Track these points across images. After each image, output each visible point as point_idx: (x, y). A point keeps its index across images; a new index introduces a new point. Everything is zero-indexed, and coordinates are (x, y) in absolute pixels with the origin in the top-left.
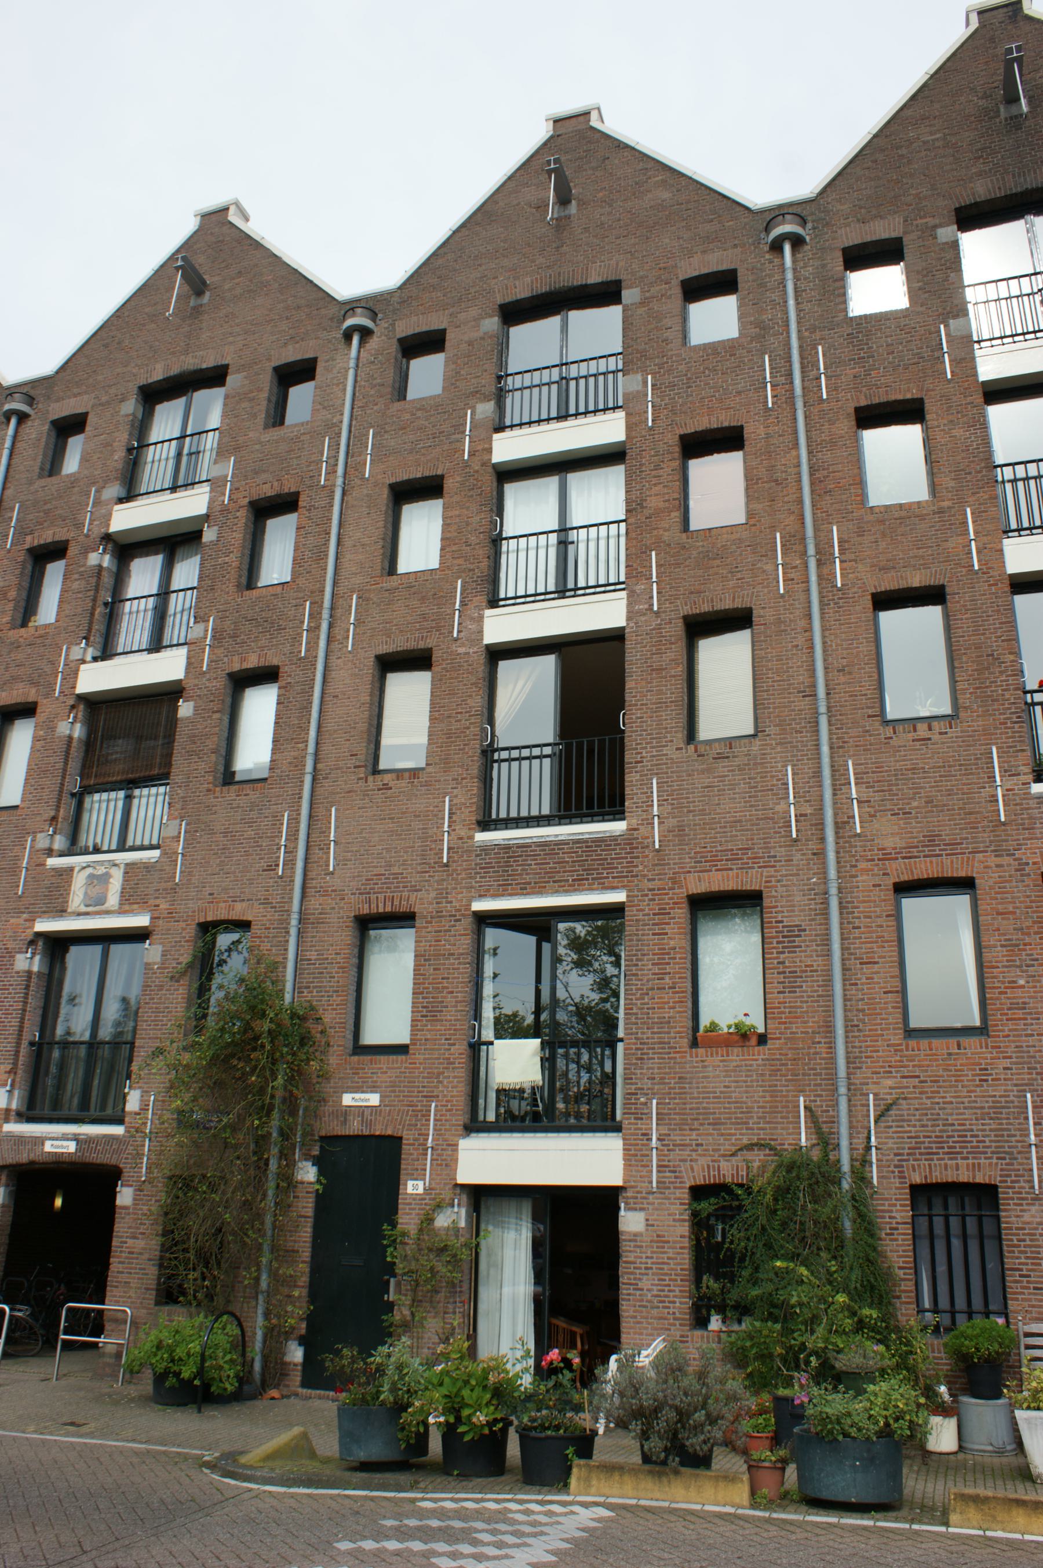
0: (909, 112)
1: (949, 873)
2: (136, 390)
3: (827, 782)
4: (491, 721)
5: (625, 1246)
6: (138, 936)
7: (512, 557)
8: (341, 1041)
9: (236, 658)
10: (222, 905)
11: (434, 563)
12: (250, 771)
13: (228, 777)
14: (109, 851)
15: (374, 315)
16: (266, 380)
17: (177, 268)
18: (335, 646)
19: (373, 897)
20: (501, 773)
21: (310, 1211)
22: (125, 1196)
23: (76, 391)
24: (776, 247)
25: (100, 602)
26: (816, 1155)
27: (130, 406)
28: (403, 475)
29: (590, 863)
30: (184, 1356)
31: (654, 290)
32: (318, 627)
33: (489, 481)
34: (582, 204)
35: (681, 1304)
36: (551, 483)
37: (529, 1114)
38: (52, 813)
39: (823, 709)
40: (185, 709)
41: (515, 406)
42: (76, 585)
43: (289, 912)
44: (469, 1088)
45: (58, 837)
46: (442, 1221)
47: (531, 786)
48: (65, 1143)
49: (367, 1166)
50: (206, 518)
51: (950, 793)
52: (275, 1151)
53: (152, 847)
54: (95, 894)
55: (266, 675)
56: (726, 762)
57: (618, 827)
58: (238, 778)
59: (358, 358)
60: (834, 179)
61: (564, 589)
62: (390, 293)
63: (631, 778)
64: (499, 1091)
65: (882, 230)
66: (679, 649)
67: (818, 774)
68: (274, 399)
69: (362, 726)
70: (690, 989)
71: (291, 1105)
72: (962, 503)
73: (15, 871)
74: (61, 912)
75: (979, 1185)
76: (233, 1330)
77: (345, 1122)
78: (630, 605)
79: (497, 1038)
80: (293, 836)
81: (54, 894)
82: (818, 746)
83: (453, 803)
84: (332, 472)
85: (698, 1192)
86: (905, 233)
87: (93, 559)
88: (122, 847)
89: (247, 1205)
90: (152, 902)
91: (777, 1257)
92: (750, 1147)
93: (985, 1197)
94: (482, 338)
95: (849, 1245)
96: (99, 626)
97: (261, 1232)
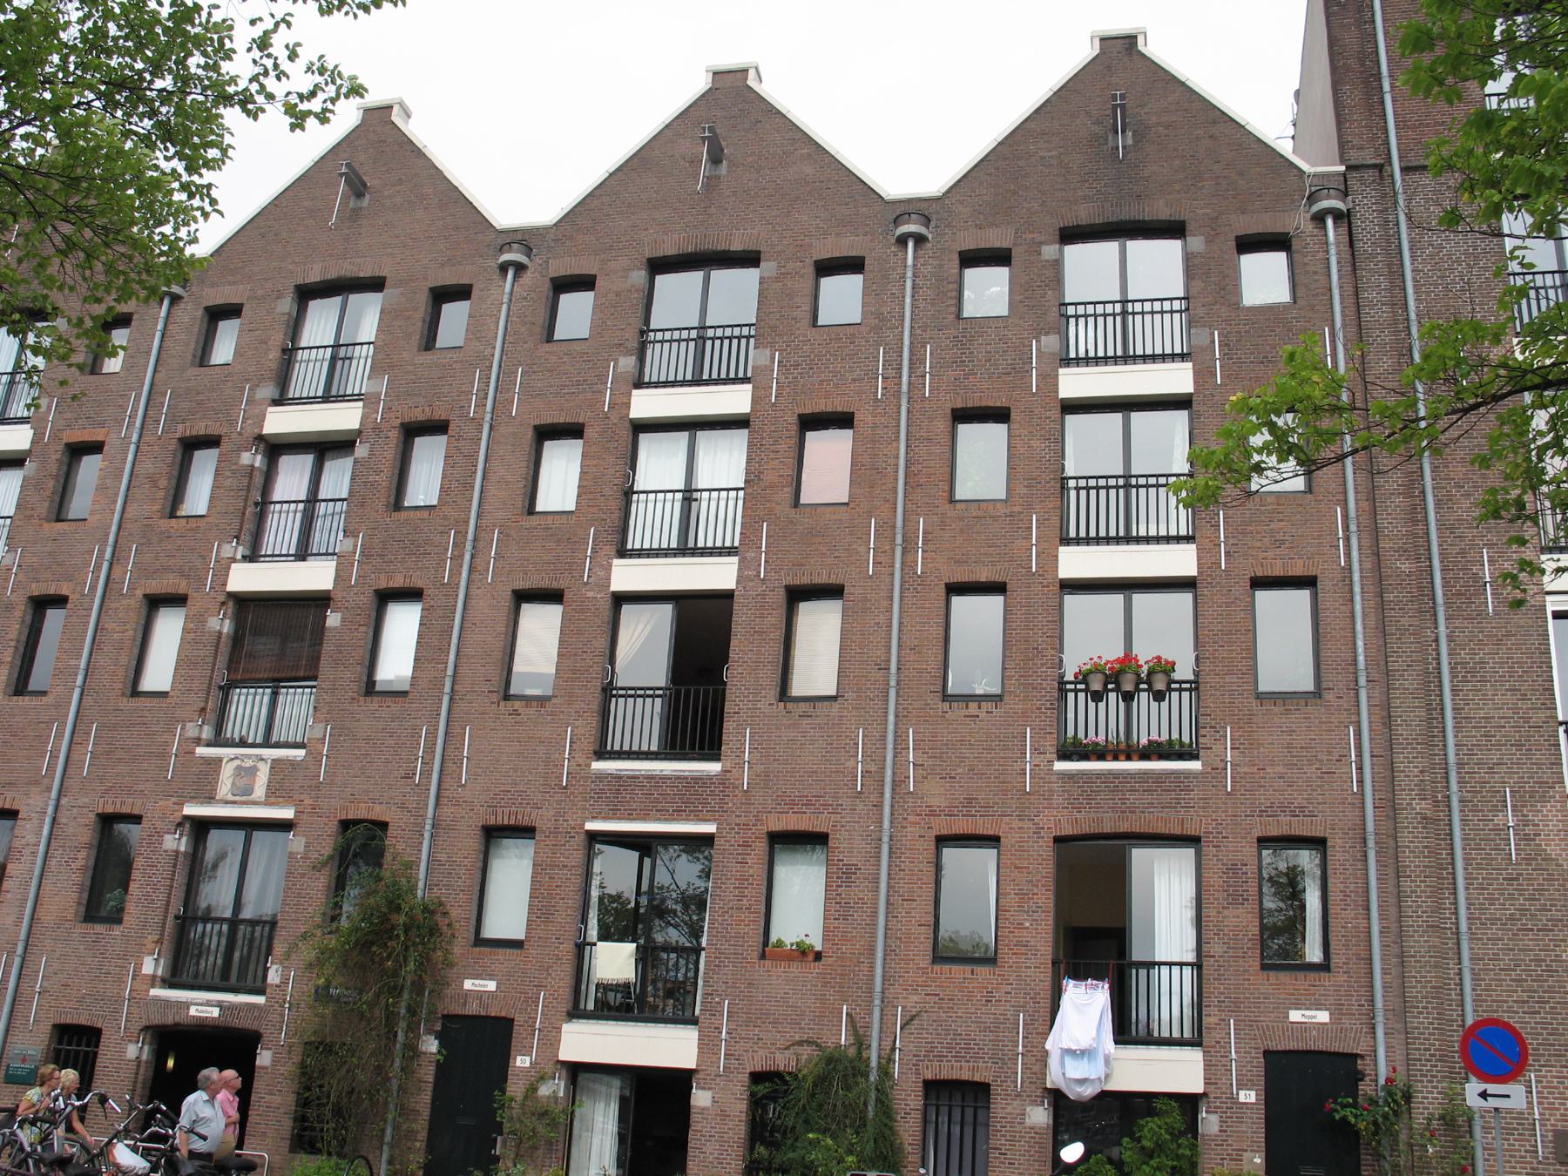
0: (1032, 125)
1: (980, 832)
2: (292, 289)
3: (890, 746)
5: (694, 1117)
6: (284, 826)
7: (642, 506)
8: (465, 934)
9: (382, 576)
11: (570, 505)
12: (391, 682)
13: (370, 688)
14: (253, 746)
16: (423, 300)
17: (341, 175)
19: (500, 811)
20: (618, 707)
24: (902, 241)
25: (250, 503)
26: (852, 1052)
27: (287, 305)
29: (689, 797)
31: (790, 266)
32: (462, 556)
33: (626, 433)
34: (732, 164)
36: (683, 437)
37: (621, 1005)
39: (893, 683)
40: (333, 619)
42: (228, 483)
43: (424, 817)
45: (206, 727)
46: (544, 1090)
47: (641, 722)
49: (482, 1043)
50: (359, 432)
52: (403, 1025)
54: (242, 784)
55: (411, 595)
57: (714, 767)
58: (378, 688)
62: (546, 229)
63: (729, 726)
65: (994, 239)
67: (884, 738)
69: (497, 655)
71: (418, 987)
72: (1030, 507)
73: (164, 756)
74: (210, 799)
77: (465, 1004)
78: (740, 569)
80: (430, 749)
81: (203, 781)
83: (576, 730)
84: (481, 405)
85: (757, 1077)
87: (246, 458)
88: (267, 744)
89: (379, 1069)
90: (297, 797)
91: (812, 1131)
92: (800, 1043)
93: (978, 1092)
95: (869, 1127)
96: (249, 526)
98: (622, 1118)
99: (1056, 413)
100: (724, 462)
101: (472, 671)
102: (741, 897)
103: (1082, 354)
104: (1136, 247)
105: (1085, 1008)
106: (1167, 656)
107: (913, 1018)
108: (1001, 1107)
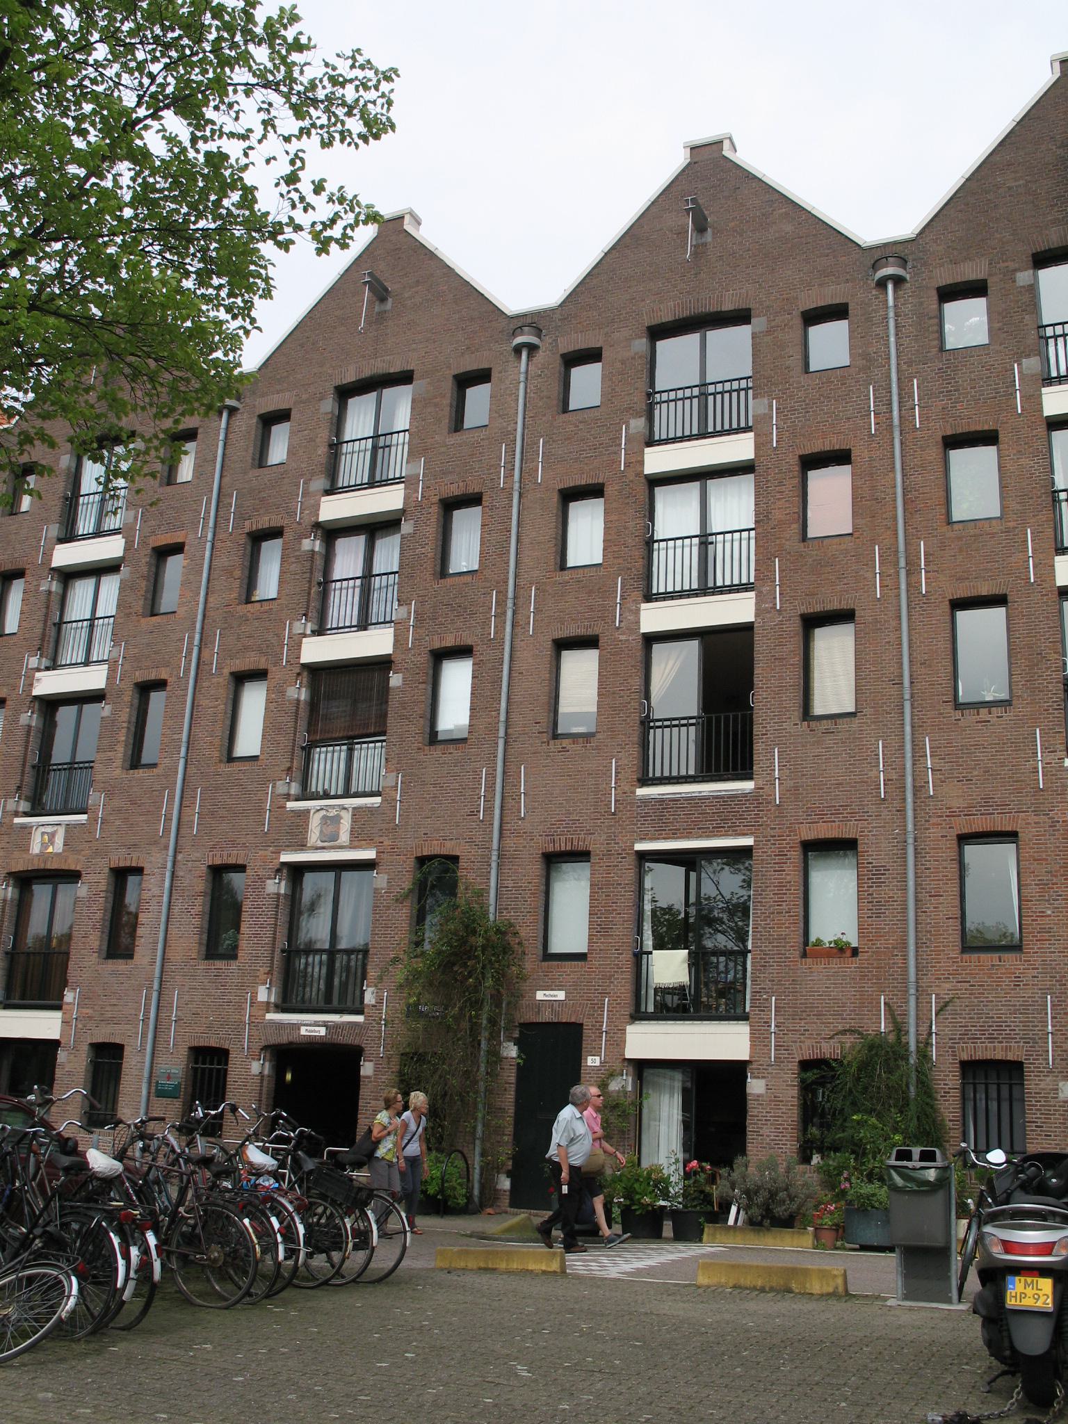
3: (909, 755)
4: (647, 695)
8: (534, 950)
13: (433, 737)
15: (538, 332)
16: (448, 386)
18: (518, 630)
21: (513, 1079)
22: (367, 1069)
23: (278, 387)
24: (882, 284)
26: (892, 1038)
27: (328, 405)
28: (570, 483)
29: (725, 814)
30: (429, 1179)
32: (504, 613)
33: (642, 488)
37: (678, 1006)
38: (288, 765)
39: (907, 696)
40: (395, 680)
43: (489, 849)
44: (634, 987)
45: (293, 784)
47: (679, 748)
48: (317, 1028)
50: (403, 511)
51: (1002, 765)
53: (372, 794)
54: (329, 831)
55: (461, 652)
56: (832, 736)
57: (748, 786)
58: (440, 737)
59: (527, 372)
60: (932, 220)
61: (705, 589)
62: (552, 310)
63: (758, 747)
64: (655, 989)
65: (970, 272)
66: (796, 643)
67: (902, 747)
68: (455, 404)
69: (544, 699)
70: (802, 913)
71: (497, 1000)
73: (261, 811)
74: (302, 846)
75: (1010, 1062)
76: (460, 1163)
79: (655, 948)
80: (491, 787)
81: (295, 831)
83: (617, 765)
84: (509, 475)
85: (805, 1065)
86: (990, 275)
87: (307, 544)
88: (347, 794)
92: (844, 1032)
93: (1012, 1071)
96: (315, 604)
97: (477, 1092)
100: (734, 507)
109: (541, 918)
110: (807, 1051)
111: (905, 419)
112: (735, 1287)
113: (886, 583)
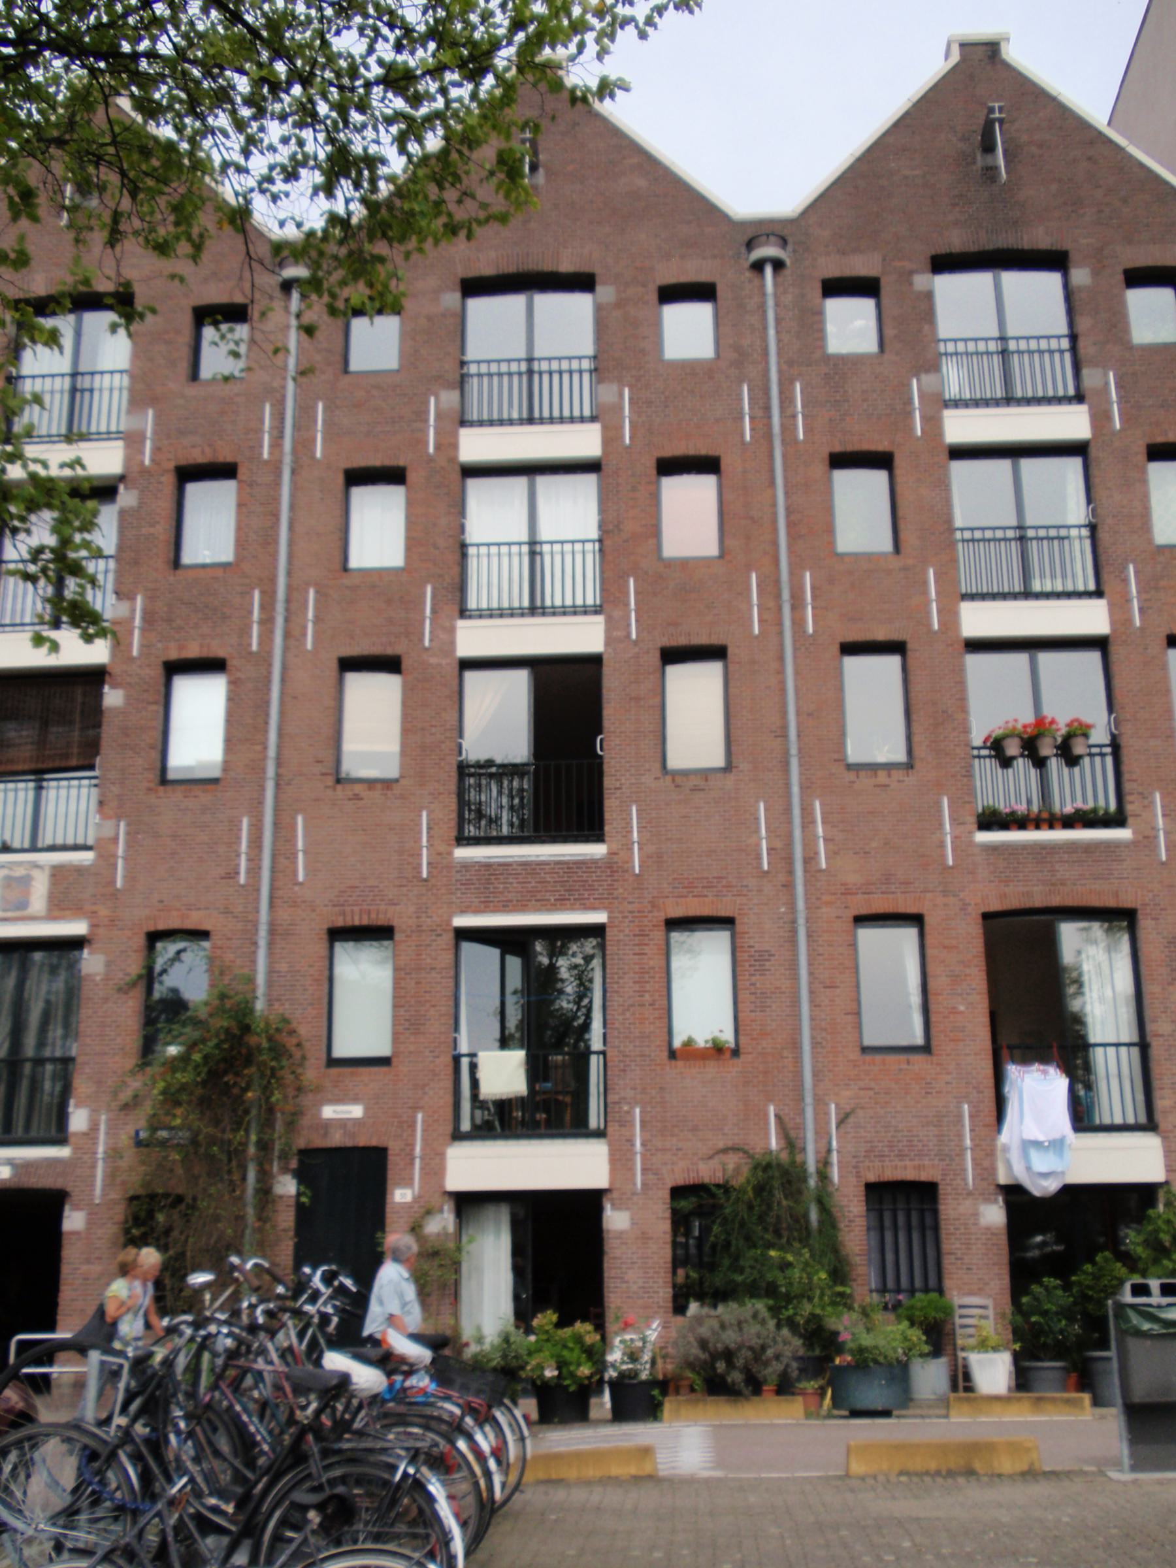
8: (316, 1057)
10: (175, 913)
12: (190, 769)
19: (348, 909)
22: (73, 1221)
24: (758, 266)
29: (570, 884)
34: (549, 174)
35: (664, 1294)
36: (521, 482)
37: (503, 1121)
39: (794, 750)
40: (112, 697)
41: (479, 399)
50: (122, 478)
63: (611, 805)
65: (860, 266)
67: (788, 810)
77: (326, 1134)
82: (788, 785)
84: (277, 443)
85: (677, 1192)
88: (34, 848)
92: (725, 1151)
93: (924, 1194)
94: (444, 315)
98: (517, 1251)
99: (457, 475)
100: (571, 512)
101: (286, 748)
102: (641, 993)
103: (576, 413)
104: (1010, 278)
105: (1039, 1091)
106: (1087, 719)
107: (847, 1116)
108: (950, 1208)
109: (325, 1011)
110: (681, 1176)
111: (788, 428)
112: (901, 1473)
113: (765, 617)
